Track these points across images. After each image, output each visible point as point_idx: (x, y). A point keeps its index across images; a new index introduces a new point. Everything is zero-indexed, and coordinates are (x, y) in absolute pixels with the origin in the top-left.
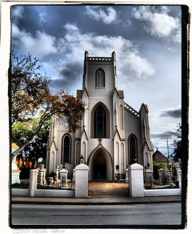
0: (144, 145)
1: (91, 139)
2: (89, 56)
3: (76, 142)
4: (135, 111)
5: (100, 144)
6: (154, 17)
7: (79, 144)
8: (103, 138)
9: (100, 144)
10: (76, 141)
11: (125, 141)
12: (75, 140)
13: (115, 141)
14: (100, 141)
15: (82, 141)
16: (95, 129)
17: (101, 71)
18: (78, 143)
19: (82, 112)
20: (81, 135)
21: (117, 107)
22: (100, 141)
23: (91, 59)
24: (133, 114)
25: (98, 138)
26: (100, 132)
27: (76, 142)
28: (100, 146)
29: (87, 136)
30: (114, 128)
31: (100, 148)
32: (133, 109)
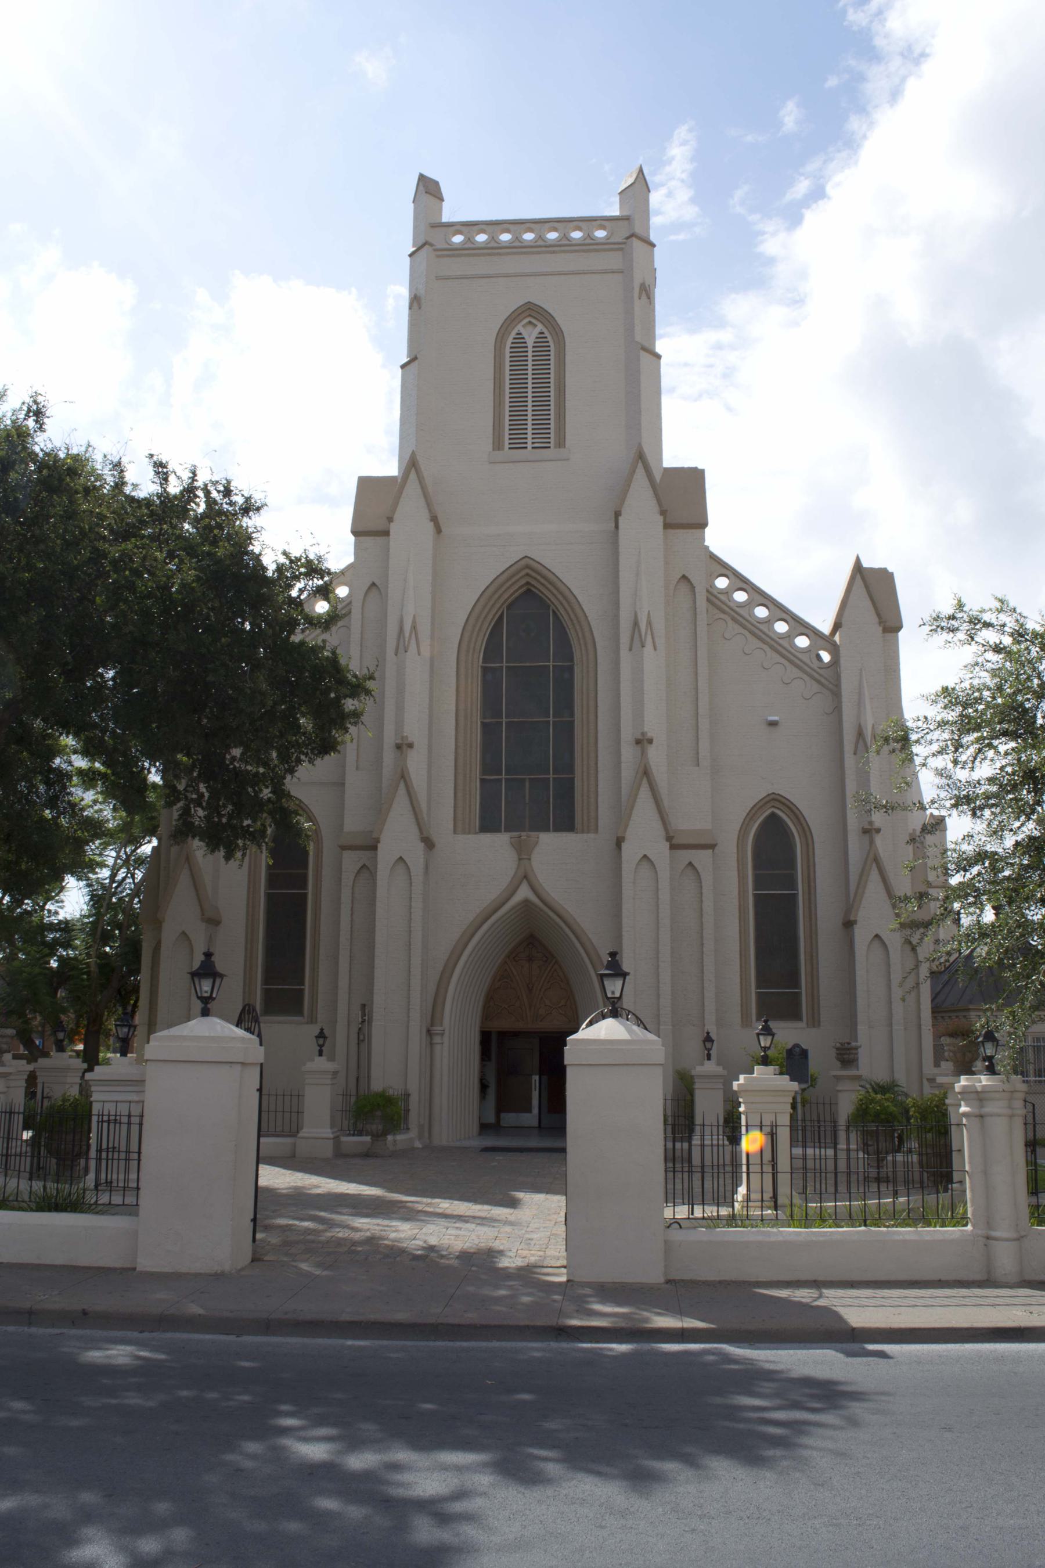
0: (863, 874)
1: (460, 837)
2: (450, 213)
3: (351, 861)
4: (800, 626)
5: (525, 877)
6: (458, 1535)
7: (368, 870)
8: (547, 829)
9: (525, 877)
10: (347, 854)
11: (710, 851)
12: (344, 848)
13: (630, 852)
14: (523, 852)
15: (386, 854)
16: (490, 764)
17: (540, 327)
18: (364, 866)
19: (112, 484)
20: (381, 810)
21: (729, 1364)
22: (523, 852)
23: (458, 239)
24: (781, 647)
25: (508, 829)
26: (527, 784)
27: (351, 861)
28: (524, 892)
29: (666, 803)
30: (628, 753)
31: (526, 902)
32: (780, 611)
